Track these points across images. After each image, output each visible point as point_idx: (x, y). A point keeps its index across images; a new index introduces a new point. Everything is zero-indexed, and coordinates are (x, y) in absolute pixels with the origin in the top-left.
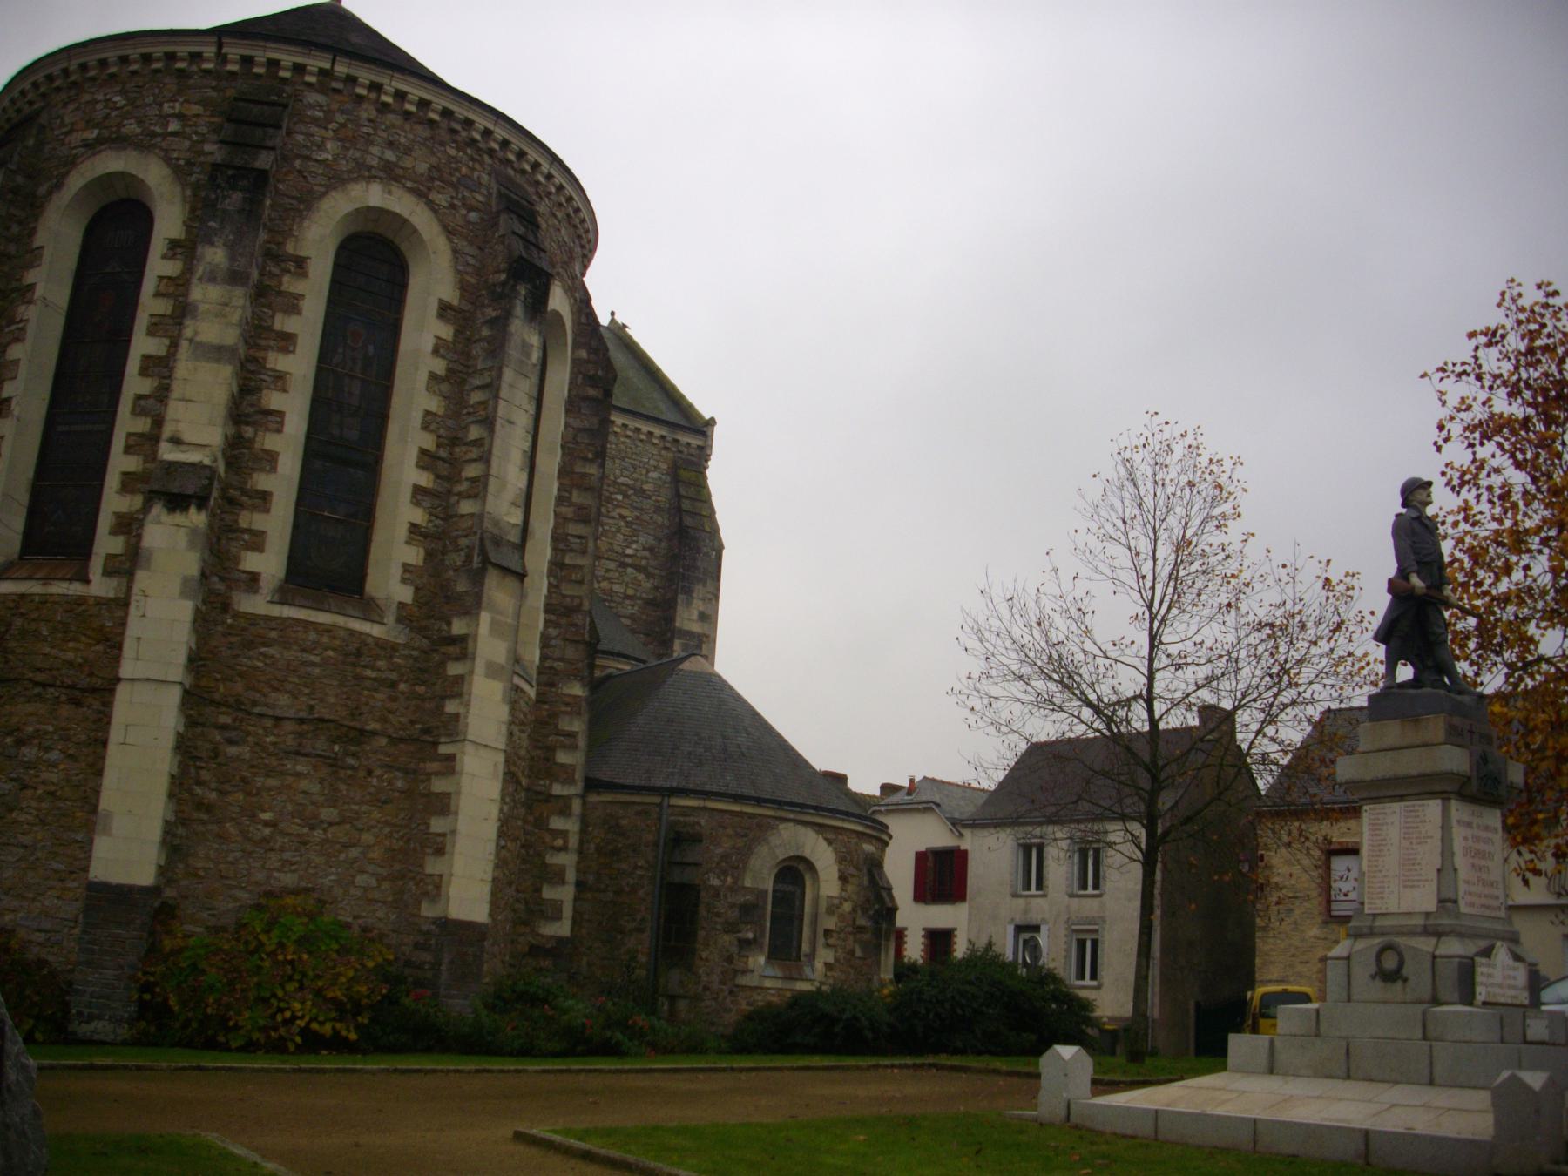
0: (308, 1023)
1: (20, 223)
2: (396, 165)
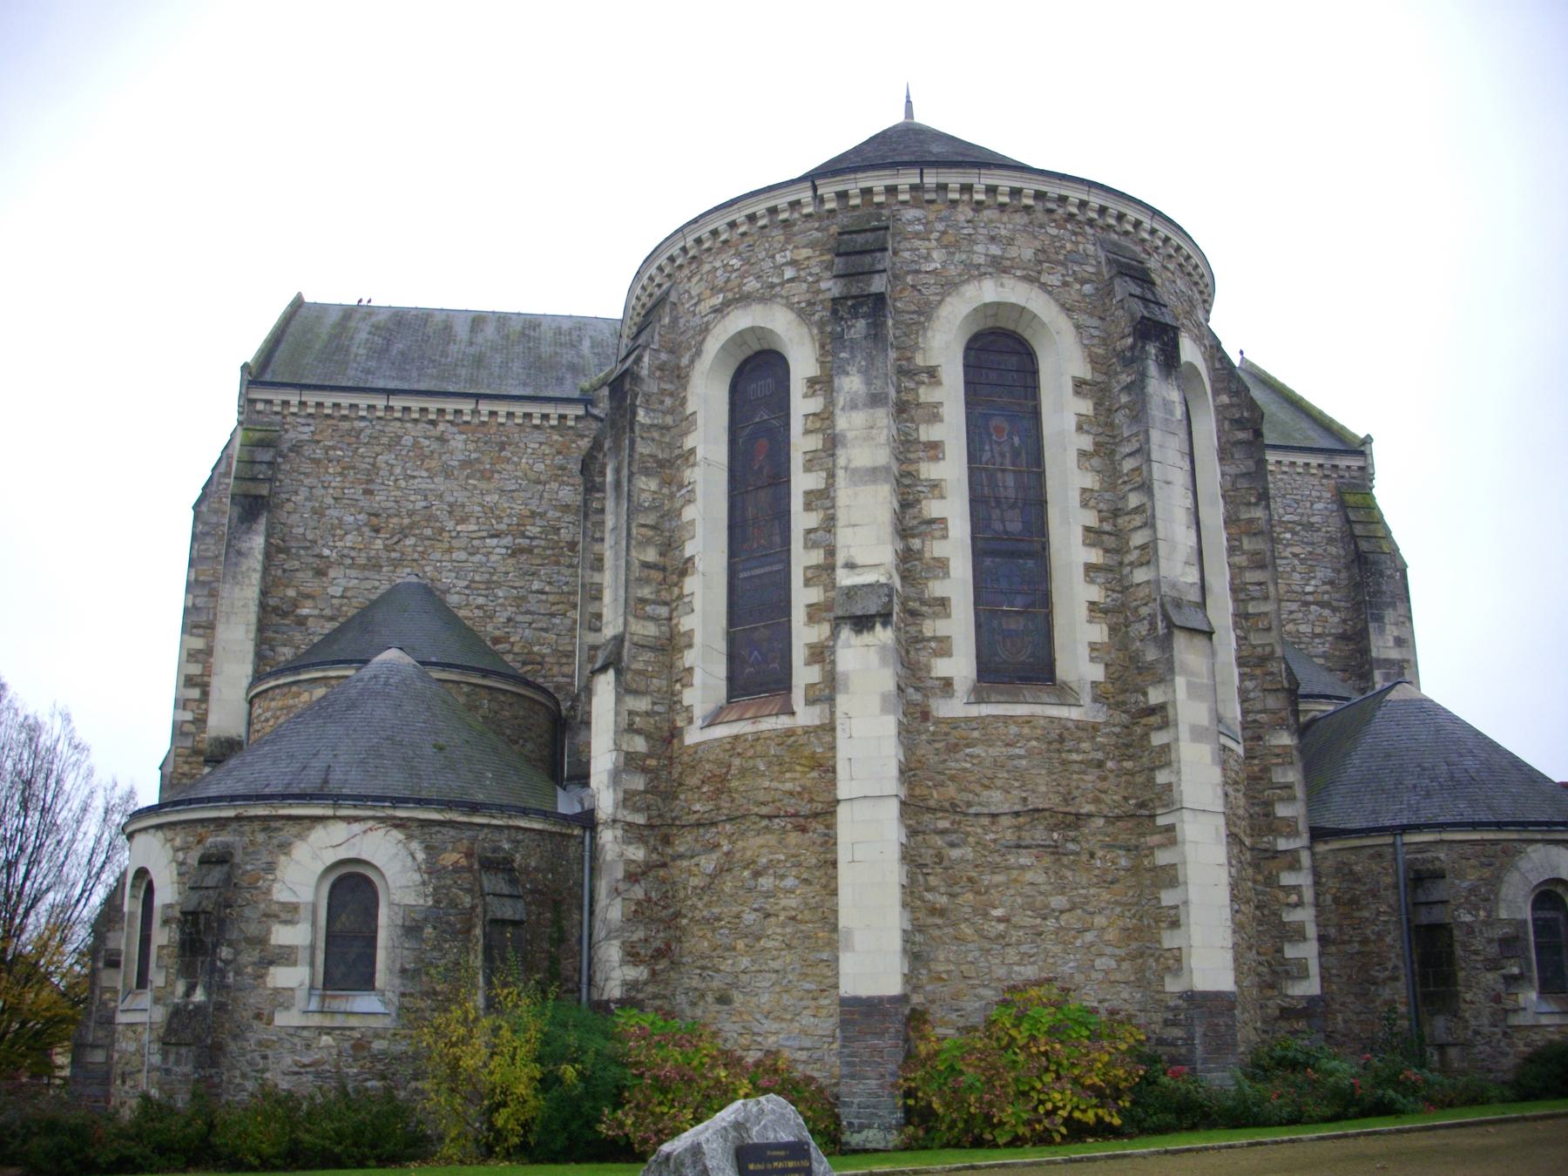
0: (1070, 1113)
1: (671, 395)
2: (1002, 258)
